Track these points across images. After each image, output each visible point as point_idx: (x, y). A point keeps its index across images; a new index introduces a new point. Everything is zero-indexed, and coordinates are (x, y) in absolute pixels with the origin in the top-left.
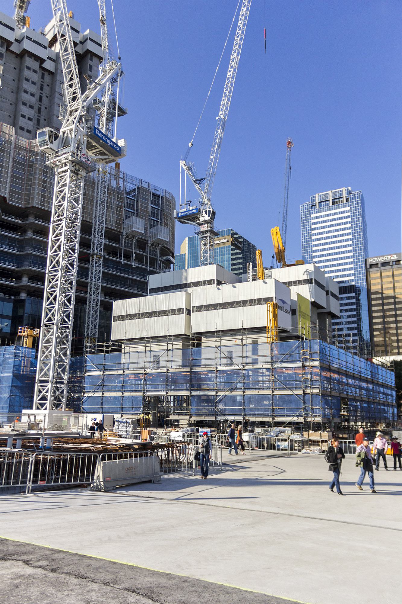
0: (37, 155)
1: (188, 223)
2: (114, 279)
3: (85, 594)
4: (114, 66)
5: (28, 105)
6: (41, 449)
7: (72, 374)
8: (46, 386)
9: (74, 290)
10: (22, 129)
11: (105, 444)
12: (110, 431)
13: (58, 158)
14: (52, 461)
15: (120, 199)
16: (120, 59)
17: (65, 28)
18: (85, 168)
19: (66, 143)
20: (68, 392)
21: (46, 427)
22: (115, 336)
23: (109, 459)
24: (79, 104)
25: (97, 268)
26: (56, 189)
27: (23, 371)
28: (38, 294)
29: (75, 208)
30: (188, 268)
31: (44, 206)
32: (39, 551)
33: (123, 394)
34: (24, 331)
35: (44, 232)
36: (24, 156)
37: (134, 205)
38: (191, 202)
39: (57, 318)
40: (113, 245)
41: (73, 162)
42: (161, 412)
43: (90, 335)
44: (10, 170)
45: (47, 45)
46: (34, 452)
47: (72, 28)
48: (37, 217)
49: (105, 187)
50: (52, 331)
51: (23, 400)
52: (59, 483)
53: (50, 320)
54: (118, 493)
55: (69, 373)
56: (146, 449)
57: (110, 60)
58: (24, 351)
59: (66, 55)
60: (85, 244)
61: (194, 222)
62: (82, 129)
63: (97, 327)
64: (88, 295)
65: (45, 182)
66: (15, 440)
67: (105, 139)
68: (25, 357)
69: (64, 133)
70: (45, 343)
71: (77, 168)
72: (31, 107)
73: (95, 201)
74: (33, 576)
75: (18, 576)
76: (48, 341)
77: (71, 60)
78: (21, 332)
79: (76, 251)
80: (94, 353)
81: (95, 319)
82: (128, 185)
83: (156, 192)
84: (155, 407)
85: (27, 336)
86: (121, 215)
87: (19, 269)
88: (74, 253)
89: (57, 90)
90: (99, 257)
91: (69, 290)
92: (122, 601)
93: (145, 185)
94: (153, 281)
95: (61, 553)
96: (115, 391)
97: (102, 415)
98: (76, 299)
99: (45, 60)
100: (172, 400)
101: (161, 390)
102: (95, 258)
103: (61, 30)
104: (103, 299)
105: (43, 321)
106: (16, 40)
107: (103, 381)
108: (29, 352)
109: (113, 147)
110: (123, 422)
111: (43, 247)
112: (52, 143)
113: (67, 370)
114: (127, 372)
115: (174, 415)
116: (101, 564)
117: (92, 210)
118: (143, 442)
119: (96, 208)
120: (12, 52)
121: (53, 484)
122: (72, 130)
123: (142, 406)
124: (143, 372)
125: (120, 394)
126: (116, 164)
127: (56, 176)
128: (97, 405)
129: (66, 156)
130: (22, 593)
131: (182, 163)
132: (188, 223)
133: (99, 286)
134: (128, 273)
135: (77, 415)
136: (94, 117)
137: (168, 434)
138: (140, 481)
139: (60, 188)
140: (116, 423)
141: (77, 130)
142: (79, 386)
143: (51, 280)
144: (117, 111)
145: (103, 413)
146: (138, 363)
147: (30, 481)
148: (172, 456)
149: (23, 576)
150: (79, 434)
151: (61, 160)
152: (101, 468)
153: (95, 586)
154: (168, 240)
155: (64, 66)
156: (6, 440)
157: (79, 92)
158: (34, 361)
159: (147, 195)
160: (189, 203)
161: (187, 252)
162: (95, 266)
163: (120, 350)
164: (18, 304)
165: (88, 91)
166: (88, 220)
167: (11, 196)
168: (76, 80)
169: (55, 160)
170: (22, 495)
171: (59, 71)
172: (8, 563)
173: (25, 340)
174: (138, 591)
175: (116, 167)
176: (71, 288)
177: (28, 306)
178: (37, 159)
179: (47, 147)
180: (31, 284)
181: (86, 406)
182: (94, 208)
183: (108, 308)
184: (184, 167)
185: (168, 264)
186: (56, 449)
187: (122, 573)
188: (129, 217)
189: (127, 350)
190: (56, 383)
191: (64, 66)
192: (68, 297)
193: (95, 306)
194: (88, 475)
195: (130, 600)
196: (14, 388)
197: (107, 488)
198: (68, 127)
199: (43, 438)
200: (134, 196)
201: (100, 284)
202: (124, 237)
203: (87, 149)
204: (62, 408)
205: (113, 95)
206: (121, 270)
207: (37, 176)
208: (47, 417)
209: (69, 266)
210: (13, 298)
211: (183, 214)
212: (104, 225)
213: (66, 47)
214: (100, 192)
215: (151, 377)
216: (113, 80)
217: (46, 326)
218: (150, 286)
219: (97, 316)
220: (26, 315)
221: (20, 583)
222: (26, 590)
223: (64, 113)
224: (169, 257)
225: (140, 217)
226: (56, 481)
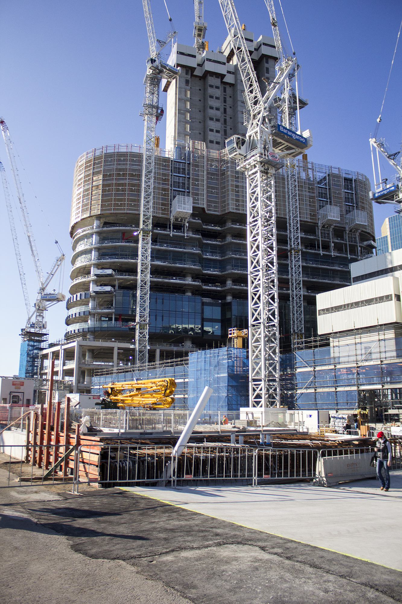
0: (227, 163)
1: (387, 203)
2: (314, 272)
3: (322, 583)
4: (290, 63)
5: (215, 131)
6: (262, 445)
7: (283, 371)
8: (260, 385)
9: (276, 288)
10: (211, 142)
11: (323, 440)
12: (326, 427)
13: (247, 162)
14: (274, 456)
15: (311, 190)
16: (294, 54)
17: (240, 42)
18: (274, 166)
19: (253, 146)
20: (281, 390)
21: (264, 424)
22: (321, 331)
23: (329, 455)
24: (261, 106)
25: (296, 263)
26: (249, 191)
27: (237, 371)
28: (243, 296)
29: (268, 206)
30: (392, 250)
31: (239, 210)
32: (273, 539)
33: (336, 389)
34: (234, 333)
35: (242, 235)
36: (216, 166)
37: (326, 194)
38: (387, 180)
39: (263, 318)
40: (310, 237)
41: (261, 162)
42: (379, 406)
43: (297, 332)
44: (205, 182)
45: (225, 61)
46: (256, 447)
47: (246, 39)
48: (234, 221)
49: (295, 181)
50: (259, 330)
51: (239, 398)
52: (283, 478)
53: (256, 319)
54: (341, 489)
55: (280, 371)
56: (365, 444)
57: (286, 57)
58: (235, 352)
59: (243, 65)
60: (282, 240)
61: (393, 200)
62: (266, 129)
63: (303, 323)
64: (290, 292)
65: (237, 186)
66: (237, 436)
67: (289, 133)
68: (237, 358)
69: (250, 137)
70: (255, 342)
71: (267, 168)
72: (218, 120)
73: (287, 196)
74: (268, 561)
75: (256, 560)
76: (257, 341)
77: (248, 69)
78: (231, 334)
79: (274, 249)
80: (302, 349)
81: (300, 322)
82: (318, 174)
83: (347, 176)
84: (371, 401)
85: (237, 337)
86: (314, 206)
87: (223, 273)
88: (273, 250)
89: (239, 99)
90: (297, 252)
91: (271, 288)
92: (361, 595)
93: (335, 171)
94: (356, 269)
95: (293, 543)
96: (327, 387)
97: (317, 411)
98: (279, 296)
99: (225, 75)
100: (389, 393)
101: (376, 384)
102: (293, 253)
103: (236, 44)
104: (306, 293)
105: (251, 321)
106: (199, 65)
107: (315, 377)
108: (240, 353)
109: (298, 140)
110: (339, 418)
111: (243, 249)
112: (240, 148)
113: (277, 368)
114: (338, 366)
115: (393, 409)
116: (334, 556)
117: (285, 205)
118: (362, 437)
119: (289, 203)
120: (196, 76)
121: (276, 478)
122: (257, 132)
123: (357, 401)
124: (355, 365)
125: (333, 389)
126: (303, 156)
127: (247, 179)
128: (311, 401)
129: (254, 158)
130: (262, 575)
131: (372, 141)
132: (387, 203)
133: (300, 281)
134: (328, 264)
135: (292, 412)
136: (277, 115)
137: (388, 429)
138: (363, 477)
139: (253, 189)
140: (332, 419)
141: (262, 131)
142: (291, 383)
143: (253, 280)
144: (297, 104)
145: (317, 409)
146: (349, 356)
147: (255, 475)
148: (395, 452)
149: (261, 560)
150: (296, 430)
151: (250, 163)
152: (322, 464)
153: (331, 578)
154: (366, 224)
155: (243, 75)
156: (230, 436)
157: (259, 95)
158: (245, 361)
159: (339, 181)
160: (385, 181)
161: (388, 234)
162: (294, 261)
163: (328, 345)
164: (226, 307)
165: (268, 92)
166: (283, 216)
167: (208, 206)
168: (256, 85)
169: (244, 164)
170: (249, 488)
171: (239, 81)
172: (246, 547)
173: (235, 342)
174: (376, 587)
175: (303, 158)
176: (274, 286)
177: (234, 308)
178: (228, 167)
179: (236, 153)
180: (235, 287)
181: (299, 402)
182: (287, 204)
183: (312, 302)
184: (375, 145)
185: (369, 250)
186: (276, 445)
187: (356, 568)
188: (323, 206)
189: (336, 344)
190: (269, 381)
191: (243, 75)
192: (271, 295)
193: (298, 301)
194: (310, 470)
195: (369, 595)
196: (230, 388)
197: (330, 483)
198: (254, 130)
199: (263, 434)
200: (325, 184)
201: (301, 279)
202: (320, 228)
203: (274, 146)
204: (276, 405)
205: (292, 90)
206: (321, 262)
207: (230, 183)
208: (264, 415)
209: (269, 264)
210: (220, 301)
211: (379, 194)
212: (299, 219)
213: (243, 58)
214: (291, 186)
215: (364, 371)
216: (291, 76)
217: (254, 326)
218: (353, 275)
219: (301, 312)
220: (233, 317)
221: (260, 566)
222: (266, 572)
223: (248, 118)
224: (370, 242)
225: (334, 205)
226: (280, 475)
